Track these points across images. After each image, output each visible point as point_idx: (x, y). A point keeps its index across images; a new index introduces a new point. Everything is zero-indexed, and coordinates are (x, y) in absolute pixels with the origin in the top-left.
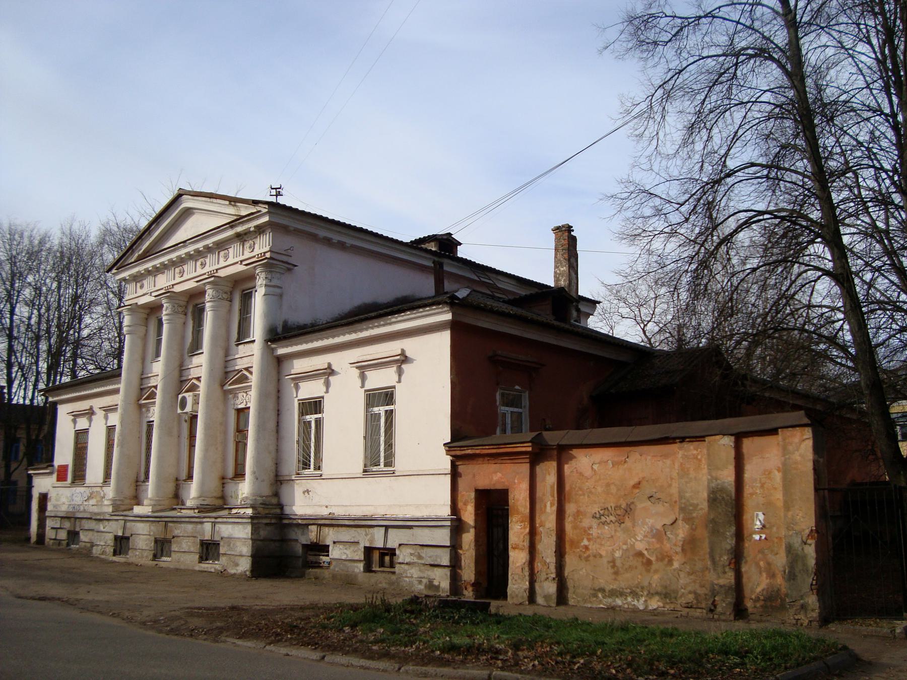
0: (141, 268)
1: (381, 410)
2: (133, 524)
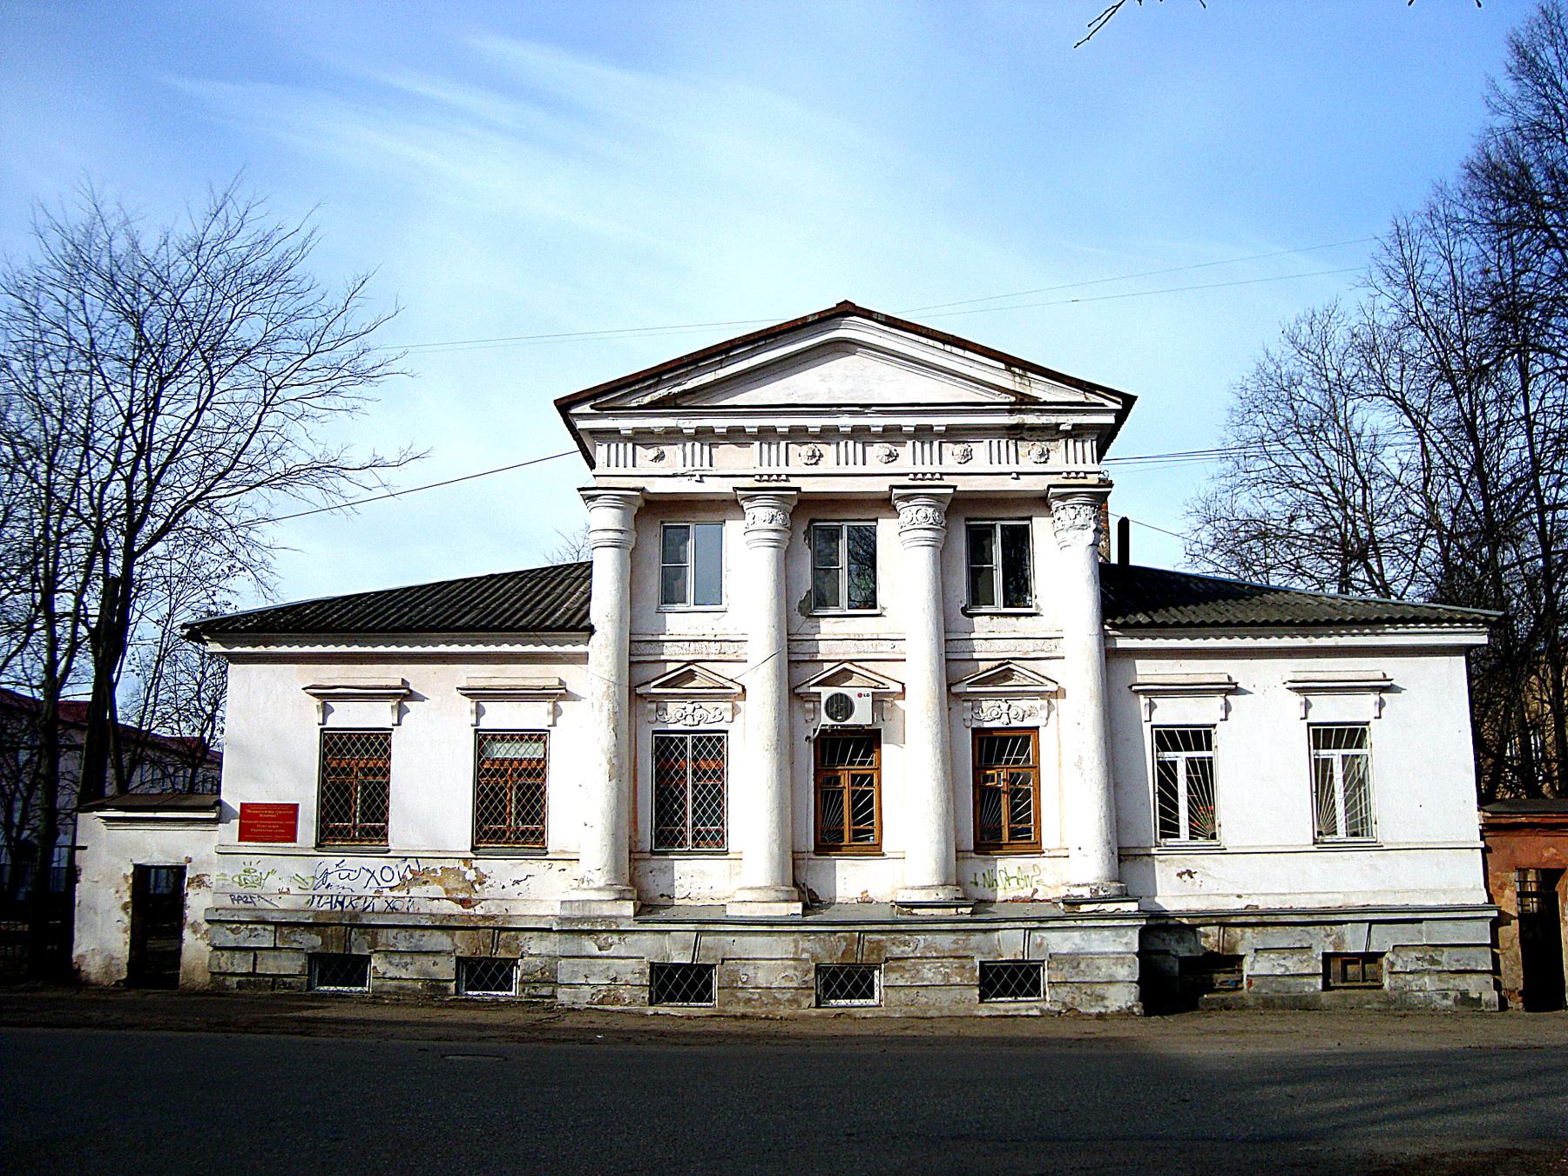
0: (657, 423)
1: (1181, 758)
2: (730, 938)
